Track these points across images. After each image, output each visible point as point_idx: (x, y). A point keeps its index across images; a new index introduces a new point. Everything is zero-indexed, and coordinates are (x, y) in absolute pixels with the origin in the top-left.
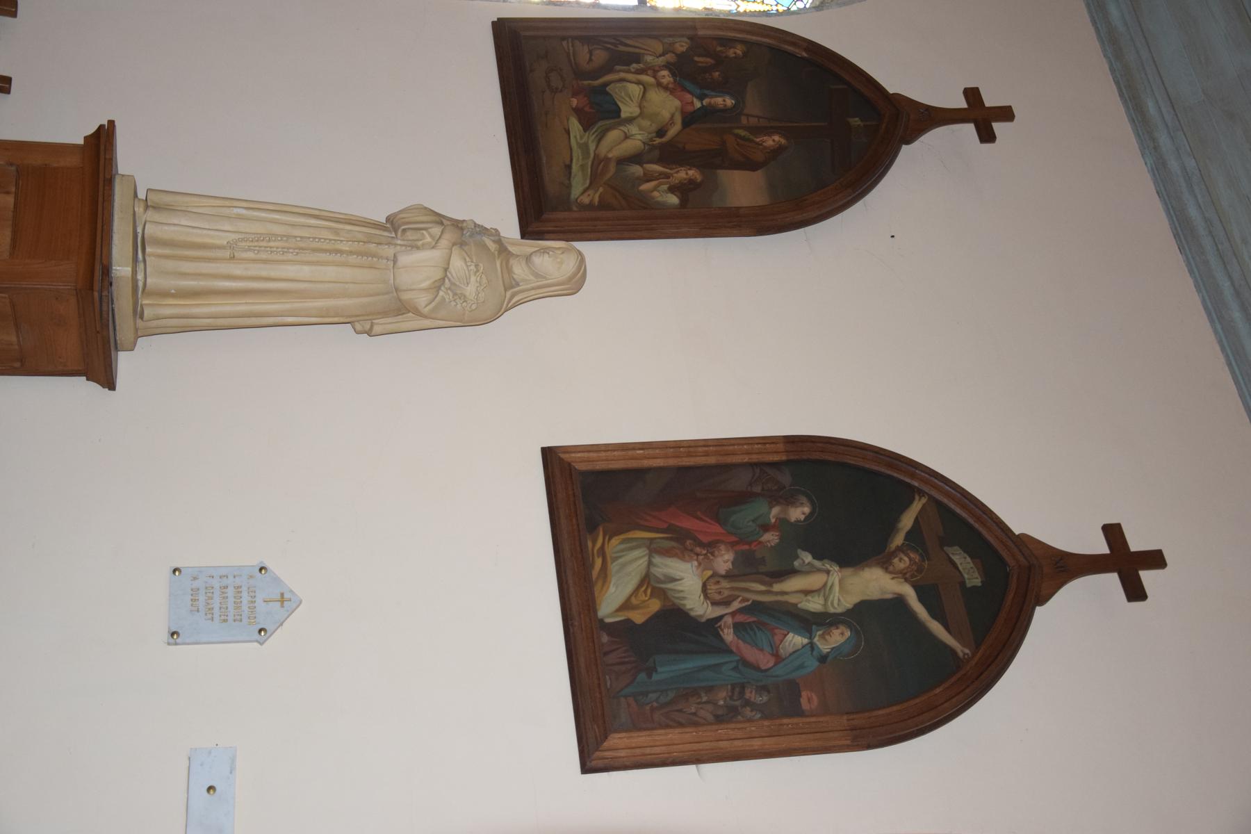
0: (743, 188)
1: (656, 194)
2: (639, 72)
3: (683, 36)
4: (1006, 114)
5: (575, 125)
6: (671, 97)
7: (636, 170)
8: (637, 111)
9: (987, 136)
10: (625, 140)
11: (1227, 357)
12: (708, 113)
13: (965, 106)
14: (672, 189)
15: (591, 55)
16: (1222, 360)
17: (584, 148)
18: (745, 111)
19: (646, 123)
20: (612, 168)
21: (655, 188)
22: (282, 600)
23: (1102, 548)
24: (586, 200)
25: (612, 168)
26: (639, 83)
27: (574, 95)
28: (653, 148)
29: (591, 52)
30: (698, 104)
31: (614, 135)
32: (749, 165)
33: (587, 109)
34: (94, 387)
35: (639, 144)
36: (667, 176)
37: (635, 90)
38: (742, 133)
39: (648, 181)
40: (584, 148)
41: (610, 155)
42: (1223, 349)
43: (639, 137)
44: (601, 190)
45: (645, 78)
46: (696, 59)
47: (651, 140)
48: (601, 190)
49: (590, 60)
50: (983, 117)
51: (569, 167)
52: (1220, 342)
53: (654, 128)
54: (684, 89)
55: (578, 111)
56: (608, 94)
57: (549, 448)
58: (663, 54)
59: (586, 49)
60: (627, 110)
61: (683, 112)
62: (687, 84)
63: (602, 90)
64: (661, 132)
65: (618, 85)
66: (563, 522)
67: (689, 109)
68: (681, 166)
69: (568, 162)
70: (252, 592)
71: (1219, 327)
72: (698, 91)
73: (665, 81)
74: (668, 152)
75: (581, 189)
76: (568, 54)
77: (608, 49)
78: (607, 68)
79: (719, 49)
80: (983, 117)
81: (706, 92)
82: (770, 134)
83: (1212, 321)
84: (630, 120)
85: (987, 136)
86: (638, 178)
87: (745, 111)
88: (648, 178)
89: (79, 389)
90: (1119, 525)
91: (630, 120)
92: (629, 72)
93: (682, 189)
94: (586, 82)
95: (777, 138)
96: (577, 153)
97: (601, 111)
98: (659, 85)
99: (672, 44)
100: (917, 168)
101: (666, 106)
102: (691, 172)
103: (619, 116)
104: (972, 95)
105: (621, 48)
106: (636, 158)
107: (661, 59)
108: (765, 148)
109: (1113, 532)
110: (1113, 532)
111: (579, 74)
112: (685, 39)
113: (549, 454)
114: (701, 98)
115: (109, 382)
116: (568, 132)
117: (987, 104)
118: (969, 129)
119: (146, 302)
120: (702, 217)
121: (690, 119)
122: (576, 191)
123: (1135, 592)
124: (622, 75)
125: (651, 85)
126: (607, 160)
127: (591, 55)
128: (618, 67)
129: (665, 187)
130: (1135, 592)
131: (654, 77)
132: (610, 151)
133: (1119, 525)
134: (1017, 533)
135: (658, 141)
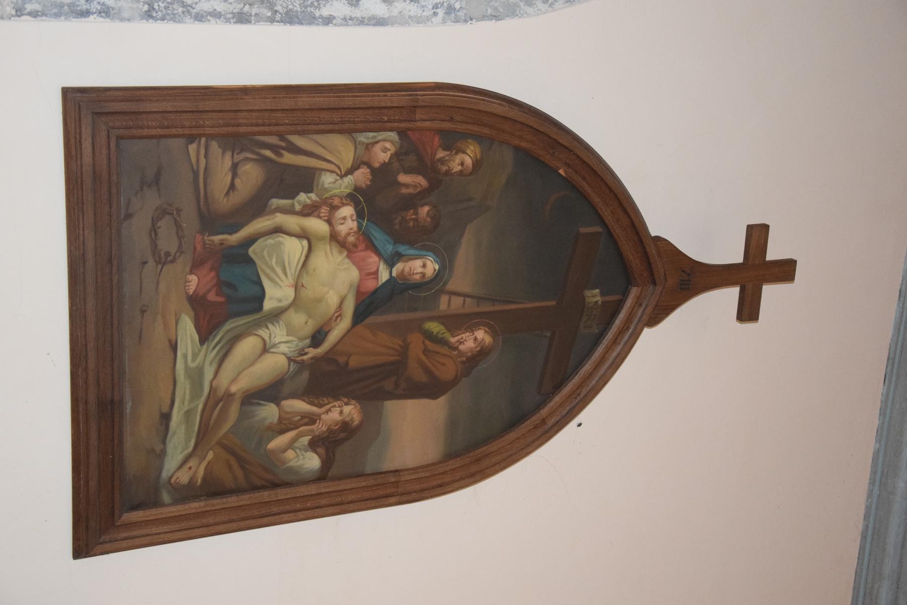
0: (413, 429)
1: (290, 454)
2: (309, 211)
3: (391, 130)
5: (187, 330)
6: (348, 263)
7: (269, 412)
8: (290, 293)
10: (266, 352)
11: (866, 528)
12: (399, 292)
14: (313, 445)
15: (235, 174)
16: (860, 527)
17: (196, 376)
18: (450, 287)
19: (298, 319)
20: (234, 410)
21: (291, 445)
24: (184, 477)
25: (234, 410)
26: (303, 235)
27: (195, 267)
28: (302, 365)
29: (235, 167)
30: (384, 276)
31: (247, 346)
32: (430, 388)
33: (212, 297)
35: (283, 360)
36: (311, 419)
37: (294, 248)
38: (435, 327)
39: (282, 432)
40: (196, 376)
41: (234, 389)
42: (866, 517)
43: (284, 348)
44: (210, 455)
45: (317, 225)
46: (403, 178)
47: (302, 353)
48: (210, 455)
49: (232, 187)
51: (166, 418)
52: (868, 508)
53: (310, 327)
54: (372, 246)
55: (196, 302)
56: (250, 261)
57: (68, 88)
58: (350, 172)
59: (228, 162)
60: (276, 294)
61: (359, 293)
62: (378, 236)
63: (240, 256)
64: (317, 338)
65: (270, 241)
67: (371, 285)
68: (336, 398)
69: (165, 410)
71: (876, 492)
72: (390, 248)
73: (343, 229)
74: (323, 375)
75: (180, 458)
76: (196, 174)
77: (264, 160)
78: (257, 206)
79: (441, 154)
81: (402, 249)
82: (471, 329)
83: (872, 482)
84: (276, 315)
86: (270, 428)
87: (450, 287)
88: (283, 427)
91: (276, 315)
92: (290, 211)
93: (328, 444)
94: (217, 238)
95: (480, 334)
96: (184, 387)
97: (232, 300)
98: (334, 237)
99: (369, 147)
101: (336, 278)
102: (347, 409)
103: (260, 308)
105: (289, 158)
106: (272, 392)
107: (349, 179)
108: (461, 354)
111: (211, 221)
112: (393, 135)
113: (81, 550)
114: (391, 264)
116: (174, 347)
117: (739, 259)
120: (352, 482)
121: (369, 304)
122: (170, 464)
124: (280, 219)
125: (322, 239)
126: (229, 396)
127: (235, 174)
128: (275, 202)
129: (305, 440)
131: (329, 222)
132: (234, 380)
135: (313, 352)
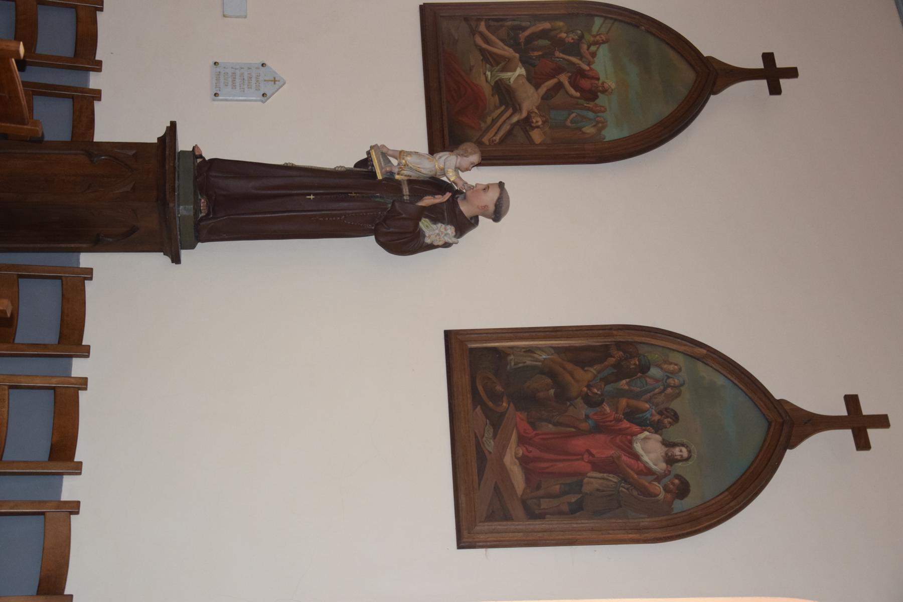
4: (792, 73)
9: (775, 90)
13: (846, 414)
22: (275, 81)
23: (843, 411)
34: (168, 259)
50: (773, 74)
66: (463, 498)
70: (258, 76)
80: (773, 74)
85: (775, 90)
89: (158, 260)
90: (772, 54)
100: (724, 110)
104: (768, 58)
109: (852, 401)
110: (852, 401)
113: (454, 341)
115: (176, 260)
117: (778, 66)
118: (847, 435)
119: (214, 174)
123: (862, 443)
130: (862, 443)
133: (772, 54)
134: (705, 55)
